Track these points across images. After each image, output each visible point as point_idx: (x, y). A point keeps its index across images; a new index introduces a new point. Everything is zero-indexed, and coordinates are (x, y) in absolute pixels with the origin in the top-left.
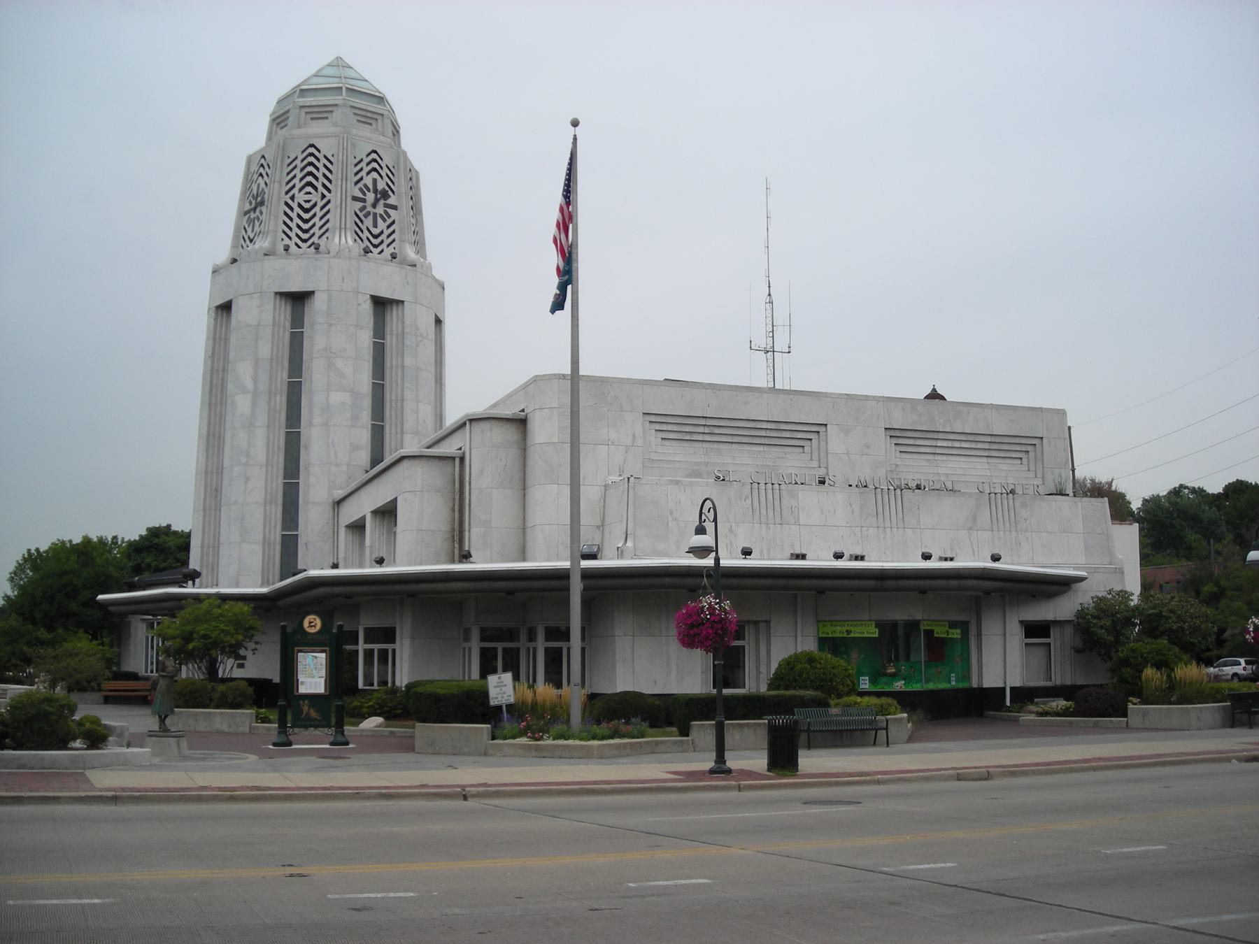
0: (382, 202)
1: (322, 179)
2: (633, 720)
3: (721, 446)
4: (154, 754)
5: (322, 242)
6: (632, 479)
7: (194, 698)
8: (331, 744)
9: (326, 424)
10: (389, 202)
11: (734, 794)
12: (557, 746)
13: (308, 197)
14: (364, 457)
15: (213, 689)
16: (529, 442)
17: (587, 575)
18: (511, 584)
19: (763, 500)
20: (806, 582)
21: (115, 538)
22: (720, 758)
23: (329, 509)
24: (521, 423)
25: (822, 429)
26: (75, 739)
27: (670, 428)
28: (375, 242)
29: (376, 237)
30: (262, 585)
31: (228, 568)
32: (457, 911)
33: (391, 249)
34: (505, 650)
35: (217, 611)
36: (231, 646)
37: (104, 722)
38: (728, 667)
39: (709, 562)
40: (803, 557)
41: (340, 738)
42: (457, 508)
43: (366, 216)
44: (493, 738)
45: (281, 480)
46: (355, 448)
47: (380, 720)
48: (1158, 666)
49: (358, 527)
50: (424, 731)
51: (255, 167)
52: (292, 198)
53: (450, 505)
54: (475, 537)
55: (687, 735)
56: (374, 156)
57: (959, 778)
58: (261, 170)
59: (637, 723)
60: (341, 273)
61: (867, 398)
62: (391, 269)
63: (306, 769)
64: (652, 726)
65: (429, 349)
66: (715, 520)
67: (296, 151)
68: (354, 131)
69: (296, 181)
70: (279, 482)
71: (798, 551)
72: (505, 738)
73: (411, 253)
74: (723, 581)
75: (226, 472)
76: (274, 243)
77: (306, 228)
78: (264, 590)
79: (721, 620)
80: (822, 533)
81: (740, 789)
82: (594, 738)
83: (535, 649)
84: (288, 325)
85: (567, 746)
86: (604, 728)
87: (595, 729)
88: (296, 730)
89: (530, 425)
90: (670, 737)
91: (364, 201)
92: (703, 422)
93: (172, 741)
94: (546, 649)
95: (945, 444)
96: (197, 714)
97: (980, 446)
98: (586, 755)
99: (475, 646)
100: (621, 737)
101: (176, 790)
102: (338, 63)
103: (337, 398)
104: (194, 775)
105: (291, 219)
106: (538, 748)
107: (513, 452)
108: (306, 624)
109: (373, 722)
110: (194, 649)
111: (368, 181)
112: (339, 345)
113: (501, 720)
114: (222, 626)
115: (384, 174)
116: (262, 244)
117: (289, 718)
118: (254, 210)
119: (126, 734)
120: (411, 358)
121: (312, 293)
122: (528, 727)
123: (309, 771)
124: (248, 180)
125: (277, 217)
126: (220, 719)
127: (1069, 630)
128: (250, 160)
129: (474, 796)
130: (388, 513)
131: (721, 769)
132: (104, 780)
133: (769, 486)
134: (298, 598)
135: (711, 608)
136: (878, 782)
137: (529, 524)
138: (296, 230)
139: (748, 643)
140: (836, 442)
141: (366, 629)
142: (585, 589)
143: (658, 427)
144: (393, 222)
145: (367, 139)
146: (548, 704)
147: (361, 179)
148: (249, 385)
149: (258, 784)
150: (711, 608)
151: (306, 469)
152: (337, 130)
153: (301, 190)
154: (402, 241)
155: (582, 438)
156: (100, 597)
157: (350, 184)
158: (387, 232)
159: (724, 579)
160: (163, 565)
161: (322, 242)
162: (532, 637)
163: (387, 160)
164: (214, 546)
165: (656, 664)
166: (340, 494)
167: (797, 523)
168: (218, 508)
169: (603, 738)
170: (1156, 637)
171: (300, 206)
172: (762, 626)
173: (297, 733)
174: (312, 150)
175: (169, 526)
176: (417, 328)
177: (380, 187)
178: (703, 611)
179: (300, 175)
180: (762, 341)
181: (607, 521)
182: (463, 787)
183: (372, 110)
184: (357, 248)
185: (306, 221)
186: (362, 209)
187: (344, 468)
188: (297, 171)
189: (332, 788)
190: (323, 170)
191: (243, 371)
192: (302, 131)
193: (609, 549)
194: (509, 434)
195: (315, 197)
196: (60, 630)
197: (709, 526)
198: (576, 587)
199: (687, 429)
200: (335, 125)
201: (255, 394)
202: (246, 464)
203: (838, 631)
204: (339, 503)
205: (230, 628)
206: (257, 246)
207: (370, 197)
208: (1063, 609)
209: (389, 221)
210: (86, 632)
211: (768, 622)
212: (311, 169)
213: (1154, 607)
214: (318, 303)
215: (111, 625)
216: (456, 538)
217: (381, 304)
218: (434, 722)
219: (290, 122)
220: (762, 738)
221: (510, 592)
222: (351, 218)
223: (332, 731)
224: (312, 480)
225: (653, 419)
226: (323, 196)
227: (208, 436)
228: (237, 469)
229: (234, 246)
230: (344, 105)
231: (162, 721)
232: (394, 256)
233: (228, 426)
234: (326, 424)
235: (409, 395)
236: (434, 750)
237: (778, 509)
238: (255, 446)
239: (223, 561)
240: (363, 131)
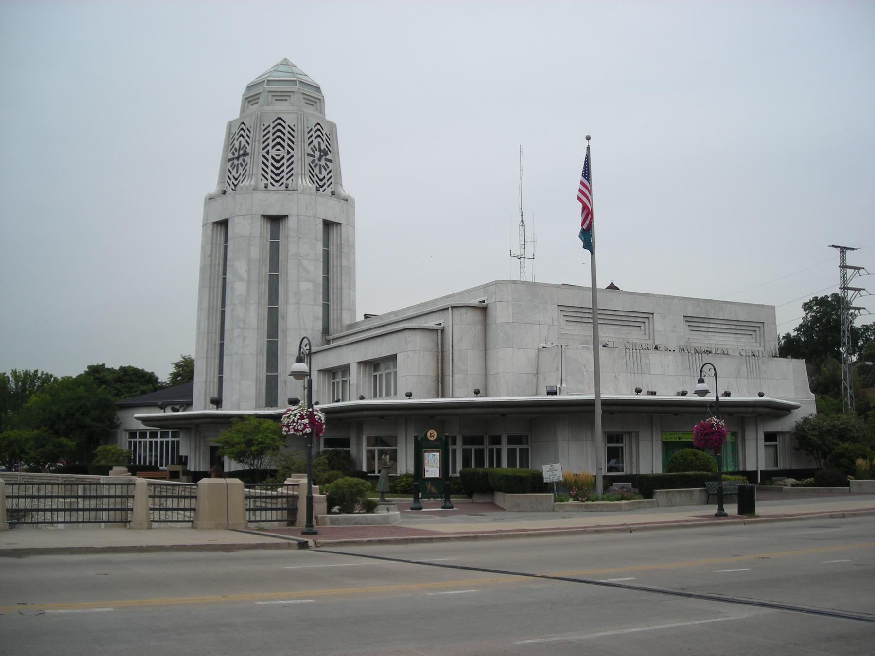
8: (443, 508)
10: (328, 157)
11: (743, 527)
13: (278, 152)
21: (36, 371)
24: (483, 309)
25: (651, 316)
27: (571, 314)
29: (278, 161)
31: (457, 391)
40: (654, 393)
41: (448, 504)
43: (315, 166)
45: (266, 339)
48: (864, 457)
51: (235, 129)
56: (318, 127)
57: (832, 517)
58: (242, 132)
61: (674, 298)
62: (333, 202)
68: (305, 110)
69: (270, 141)
70: (264, 340)
71: (680, 390)
77: (278, 172)
80: (667, 381)
83: (499, 451)
84: (269, 237)
89: (490, 311)
91: (313, 156)
95: (713, 326)
97: (731, 327)
98: (619, 509)
102: (285, 62)
103: (305, 286)
105: (267, 167)
107: (479, 328)
108: (428, 435)
118: (238, 159)
121: (284, 217)
125: (257, 164)
127: (787, 437)
128: (230, 125)
129: (635, 530)
131: (721, 514)
134: (341, 415)
135: (718, 425)
136: (801, 519)
138: (271, 174)
140: (659, 324)
143: (565, 314)
148: (245, 276)
149: (114, 545)
152: (295, 108)
153: (273, 147)
154: (336, 183)
157: (306, 145)
158: (327, 177)
159: (717, 407)
167: (650, 373)
170: (844, 441)
171: (273, 158)
172: (633, 434)
174: (280, 121)
175: (104, 365)
176: (349, 241)
179: (272, 138)
183: (313, 96)
184: (313, 187)
185: (278, 168)
186: (313, 161)
188: (270, 135)
190: (288, 135)
192: (269, 108)
194: (472, 317)
200: (293, 105)
201: (249, 281)
202: (244, 328)
203: (674, 438)
207: (317, 154)
208: (787, 424)
211: (637, 433)
213: (843, 424)
214: (292, 222)
218: (519, 493)
225: (563, 309)
226: (289, 152)
227: (209, 309)
228: (237, 332)
230: (298, 92)
232: (333, 194)
234: (298, 303)
235: (344, 284)
236: (518, 508)
240: (309, 110)
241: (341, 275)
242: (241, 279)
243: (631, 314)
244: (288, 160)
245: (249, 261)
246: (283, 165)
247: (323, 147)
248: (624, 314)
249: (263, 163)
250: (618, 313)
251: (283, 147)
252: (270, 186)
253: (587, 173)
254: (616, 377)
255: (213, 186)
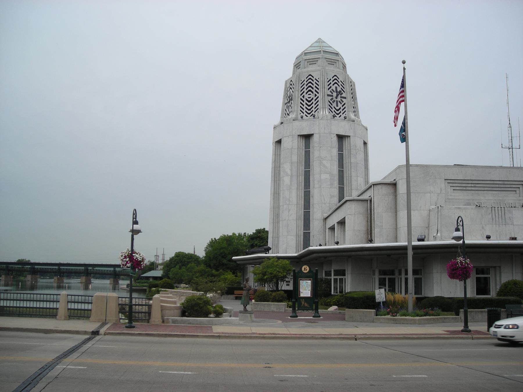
0: (339, 96)
1: (315, 88)
2: (435, 308)
3: (480, 192)
4: (240, 320)
5: (316, 114)
6: (440, 207)
7: (263, 298)
8: (313, 317)
9: (320, 187)
10: (342, 96)
12: (402, 319)
13: (309, 96)
14: (336, 199)
15: (271, 295)
16: (398, 193)
17: (415, 248)
18: (389, 252)
19: (497, 215)
20: (515, 250)
21: (245, 233)
22: (466, 325)
23: (322, 221)
24: (394, 185)
26: (211, 314)
27: (456, 185)
28: (338, 112)
29: (338, 110)
30: (296, 253)
32: (319, 383)
33: (344, 115)
34: (389, 278)
35: (276, 263)
36: (281, 277)
37: (224, 307)
38: (482, 287)
39: (461, 242)
40: (515, 239)
42: (369, 221)
43: (333, 102)
44: (377, 315)
46: (332, 196)
47: (336, 307)
49: (332, 229)
50: (348, 312)
51: (288, 85)
52: (303, 97)
53: (366, 219)
54: (376, 231)
55: (458, 315)
56: (335, 77)
59: (437, 310)
60: (324, 126)
62: (345, 123)
63: (302, 327)
64: (443, 310)
65: (361, 155)
66: (463, 225)
67: (304, 78)
68: (327, 68)
71: (513, 236)
72: (382, 315)
73: (352, 116)
74: (467, 250)
75: (281, 207)
76: (297, 115)
77: (309, 108)
78: (296, 255)
79: (465, 268)
81: (473, 339)
82: (418, 316)
83: (401, 278)
84: (304, 148)
85: (406, 319)
86: (422, 312)
87: (418, 312)
88: (299, 311)
89: (397, 186)
90: (451, 316)
91: (332, 96)
92: (471, 182)
93: (248, 315)
94: (379, 278)
96: (264, 304)
99: (377, 277)
100: (430, 315)
101: (243, 334)
102: (320, 41)
103: (324, 176)
104: (289, 329)
106: (394, 320)
107: (391, 197)
108: (303, 269)
109: (333, 308)
110: (267, 279)
111: (333, 88)
112: (324, 156)
113: (380, 308)
114: (278, 269)
115: (340, 85)
116: (292, 116)
117: (296, 306)
119: (232, 312)
120: (355, 158)
121: (312, 135)
122: (391, 311)
123: (299, 327)
124: (286, 91)
125: (298, 105)
126: (273, 306)
128: (286, 82)
129: (359, 339)
130: (342, 223)
131: (466, 330)
132: (217, 329)
133: (500, 208)
135: (461, 262)
137: (398, 227)
139: (491, 276)
141: (334, 270)
142: (414, 254)
143: (451, 185)
144: (345, 104)
145: (332, 71)
146: (400, 301)
147: (331, 87)
148: (289, 172)
150: (461, 262)
151: (313, 205)
155: (412, 190)
156: (233, 258)
158: (342, 108)
160: (262, 244)
161: (316, 114)
162: (400, 274)
163: (341, 79)
164: (277, 237)
165: (443, 286)
166: (326, 215)
168: (278, 222)
169: (421, 316)
173: (299, 312)
174: (310, 77)
175: (264, 229)
176: (356, 147)
177: (338, 90)
178: (458, 264)
179: (306, 88)
180: (507, 144)
181: (430, 225)
182: (355, 335)
183: (334, 59)
186: (331, 99)
187: (328, 205)
188: (305, 86)
189: (304, 334)
191: (287, 167)
193: (431, 237)
194: (388, 190)
195: (312, 96)
196: (221, 270)
197: (461, 228)
198: (410, 253)
199: (464, 185)
200: (319, 66)
201: (292, 176)
202: (289, 204)
204: (326, 219)
205: (281, 270)
206: (290, 117)
207: (335, 94)
209: (343, 104)
210: (231, 271)
211: (500, 267)
212: (310, 84)
214: (315, 138)
215: (240, 268)
216: (369, 233)
217: (341, 138)
219: (301, 66)
220: (485, 316)
221: (389, 255)
222: (327, 103)
223: (314, 312)
224: (315, 210)
225: (449, 181)
226: (316, 95)
228: (285, 206)
229: (282, 117)
231: (245, 307)
232: (345, 118)
233: (281, 189)
234: (320, 187)
236: (353, 320)
237: (503, 218)
238: (292, 196)
239: (281, 243)
240: (330, 68)
241: (351, 168)
242: (287, 175)
243: (506, 183)
244: (315, 100)
245: (292, 163)
246: (313, 103)
247: (339, 89)
248: (500, 183)
249: (301, 103)
250: (495, 182)
251: (313, 93)
252: (305, 117)
253: (403, 85)
254: (483, 228)
255: (277, 121)
